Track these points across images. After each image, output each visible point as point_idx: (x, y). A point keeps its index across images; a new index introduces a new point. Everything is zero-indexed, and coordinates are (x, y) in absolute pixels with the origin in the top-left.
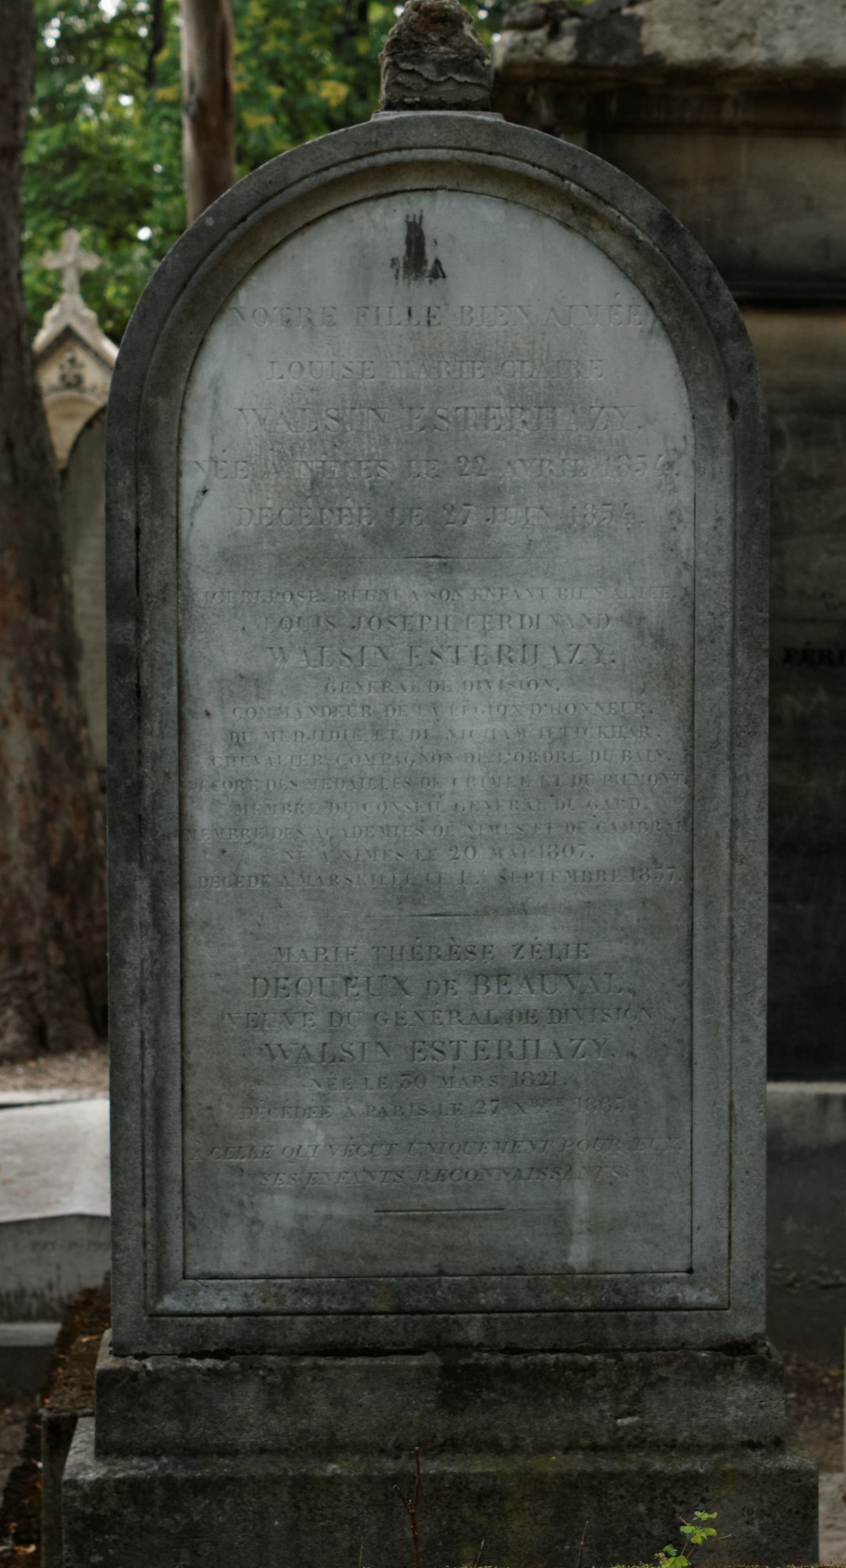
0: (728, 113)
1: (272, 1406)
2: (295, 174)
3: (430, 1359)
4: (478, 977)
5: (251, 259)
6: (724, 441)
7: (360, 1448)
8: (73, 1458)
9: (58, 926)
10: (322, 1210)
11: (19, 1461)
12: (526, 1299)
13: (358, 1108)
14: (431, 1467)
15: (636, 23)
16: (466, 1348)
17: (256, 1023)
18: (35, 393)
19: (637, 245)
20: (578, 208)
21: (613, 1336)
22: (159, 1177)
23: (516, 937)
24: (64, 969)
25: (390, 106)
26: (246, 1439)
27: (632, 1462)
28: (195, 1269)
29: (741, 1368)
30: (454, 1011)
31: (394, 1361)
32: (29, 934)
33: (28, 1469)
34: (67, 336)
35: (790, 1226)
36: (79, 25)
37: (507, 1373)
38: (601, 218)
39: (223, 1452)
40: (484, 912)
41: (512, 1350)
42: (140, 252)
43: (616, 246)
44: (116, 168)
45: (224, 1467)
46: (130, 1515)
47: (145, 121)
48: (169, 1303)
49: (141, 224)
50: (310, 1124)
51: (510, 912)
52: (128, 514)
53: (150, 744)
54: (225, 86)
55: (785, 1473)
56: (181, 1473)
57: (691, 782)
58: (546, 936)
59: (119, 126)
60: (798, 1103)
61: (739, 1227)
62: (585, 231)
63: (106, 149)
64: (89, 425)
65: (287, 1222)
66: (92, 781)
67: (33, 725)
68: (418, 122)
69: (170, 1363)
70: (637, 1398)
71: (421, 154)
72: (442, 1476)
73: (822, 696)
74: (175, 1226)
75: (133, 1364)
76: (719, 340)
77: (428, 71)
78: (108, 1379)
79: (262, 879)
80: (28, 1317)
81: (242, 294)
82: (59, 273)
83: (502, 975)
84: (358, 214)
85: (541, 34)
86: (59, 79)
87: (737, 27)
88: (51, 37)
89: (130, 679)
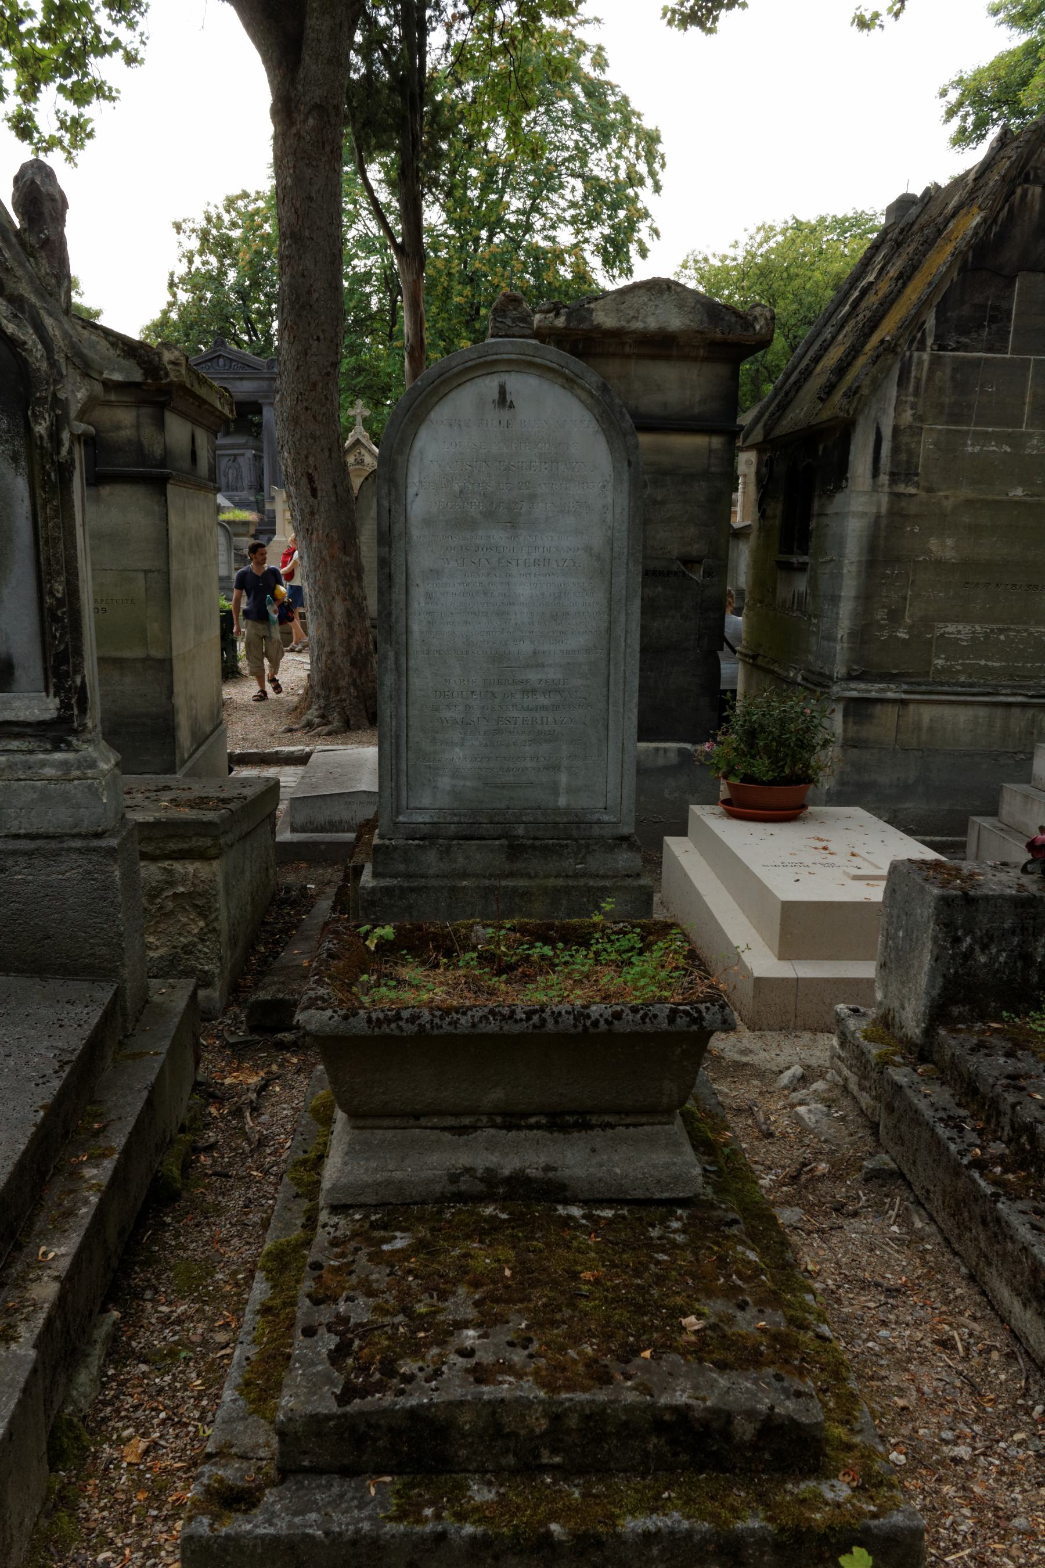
0: (627, 350)
1: (441, 859)
2: (454, 364)
3: (504, 842)
4: (525, 692)
5: (435, 399)
6: (626, 477)
7: (476, 876)
8: (363, 878)
9: (354, 680)
10: (462, 783)
11: (341, 883)
12: (541, 819)
13: (476, 743)
14: (504, 883)
15: (590, 311)
16: (517, 837)
17: (437, 709)
18: (345, 464)
19: (592, 396)
20: (568, 379)
21: (575, 833)
22: (398, 770)
23: (540, 677)
24: (357, 697)
25: (493, 336)
26: (431, 872)
27: (582, 882)
28: (411, 806)
29: (625, 846)
30: (514, 705)
31: (489, 842)
32: (343, 683)
33: (344, 886)
34: (358, 442)
35: (642, 798)
36: (362, 315)
37: (533, 847)
38: (578, 384)
39: (422, 876)
40: (527, 666)
41: (535, 838)
42: (386, 410)
43: (584, 395)
44: (377, 375)
45: (423, 882)
46: (386, 900)
47: (389, 355)
48: (401, 819)
49: (387, 399)
50: (457, 750)
51: (537, 666)
52: (386, 504)
53: (394, 597)
54: (422, 340)
55: (640, 887)
56: (406, 885)
57: (610, 615)
58: (551, 676)
59: (378, 358)
60: (647, 750)
61: (625, 791)
62: (571, 390)
63: (373, 367)
64: (366, 479)
65: (448, 788)
66: (368, 623)
67: (344, 600)
68: (504, 343)
69: (402, 842)
70: (584, 857)
71: (505, 356)
72: (507, 887)
73: (660, 589)
74: (404, 789)
75: (387, 842)
76: (625, 435)
77: (509, 322)
78: (377, 848)
79: (439, 652)
80: (343, 831)
81: (432, 414)
82: (354, 417)
83: (533, 691)
84: (479, 381)
85: (552, 315)
86: (354, 337)
87: (632, 313)
88: (350, 318)
89: (386, 571)
